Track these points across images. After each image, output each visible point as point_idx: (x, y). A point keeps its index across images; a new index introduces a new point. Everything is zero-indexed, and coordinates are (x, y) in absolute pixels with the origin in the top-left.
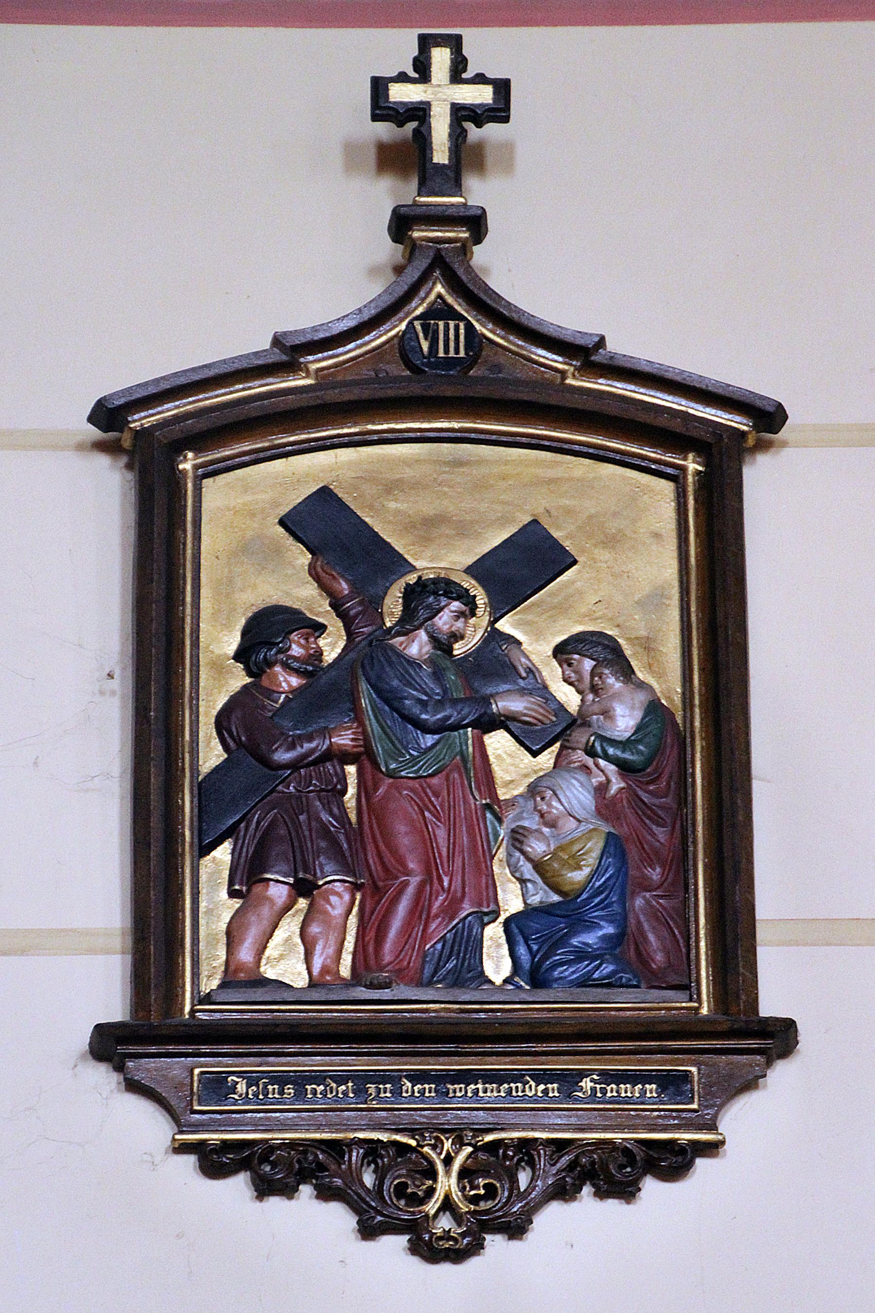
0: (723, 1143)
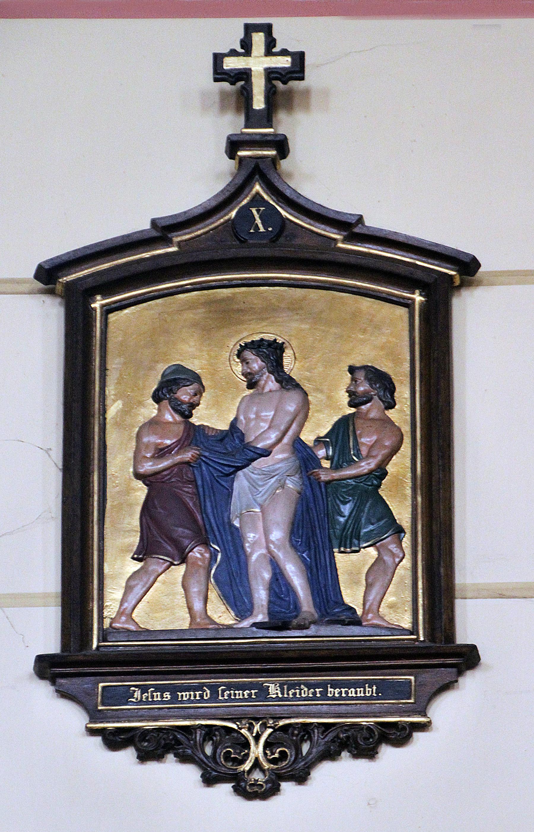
0: (430, 722)
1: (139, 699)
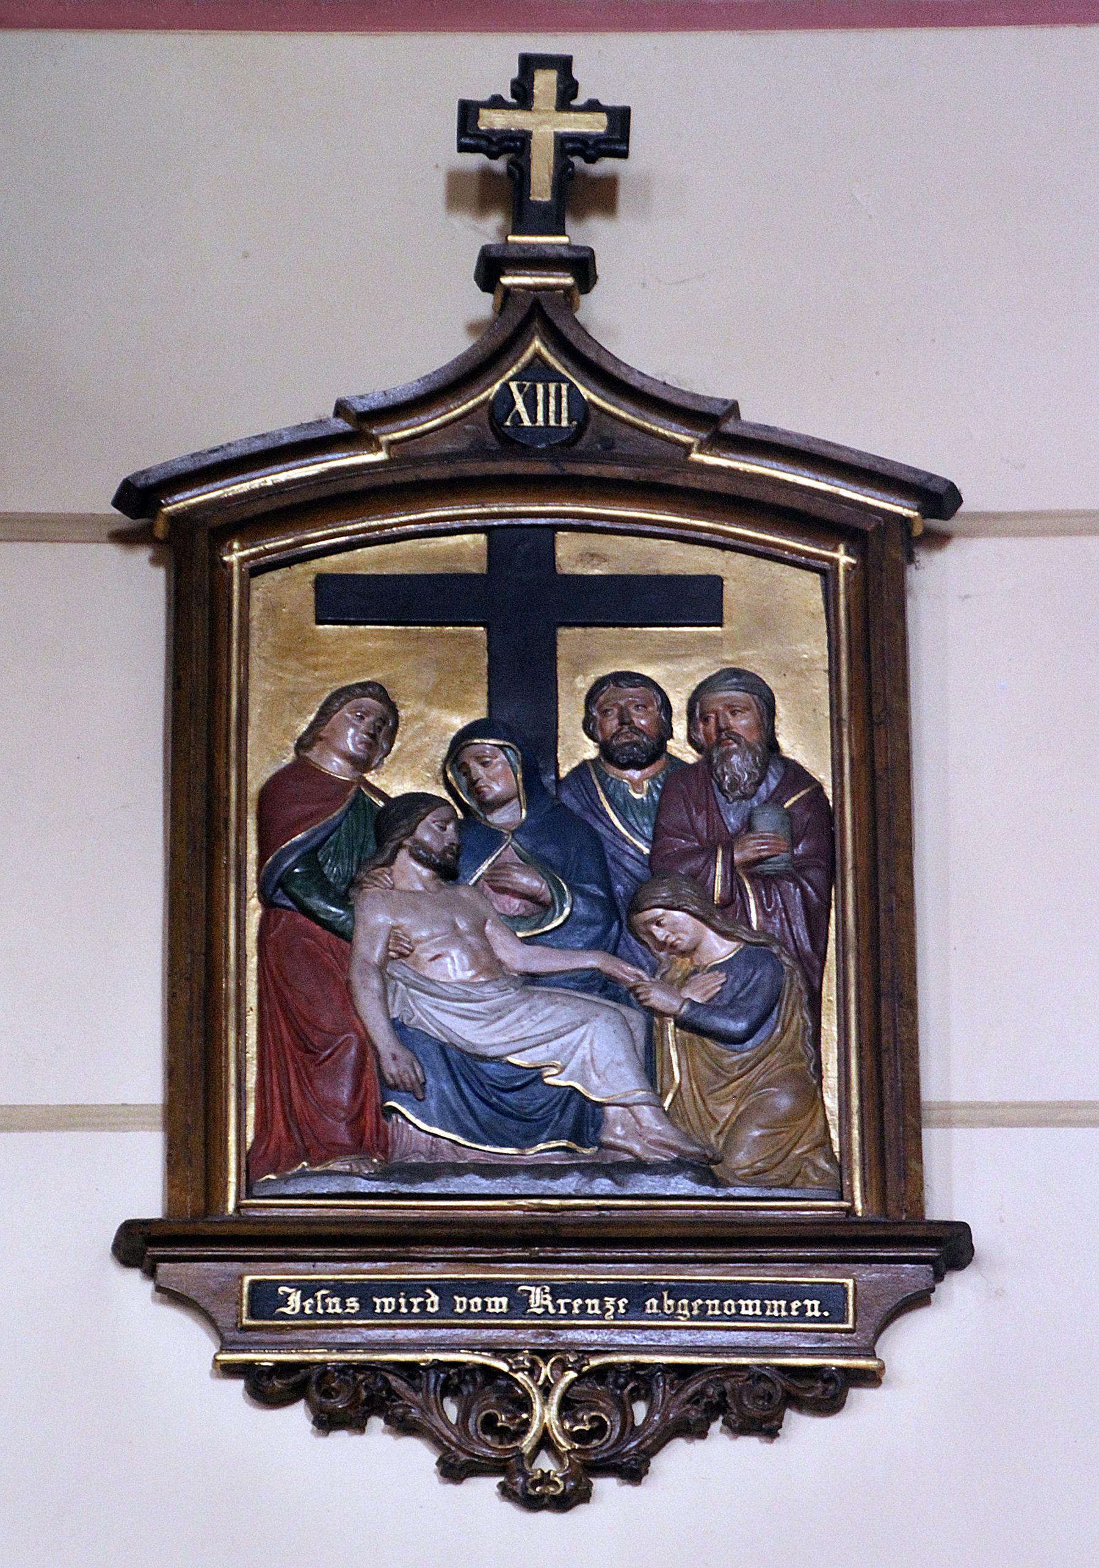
0: (882, 1368)
1: (297, 1310)
